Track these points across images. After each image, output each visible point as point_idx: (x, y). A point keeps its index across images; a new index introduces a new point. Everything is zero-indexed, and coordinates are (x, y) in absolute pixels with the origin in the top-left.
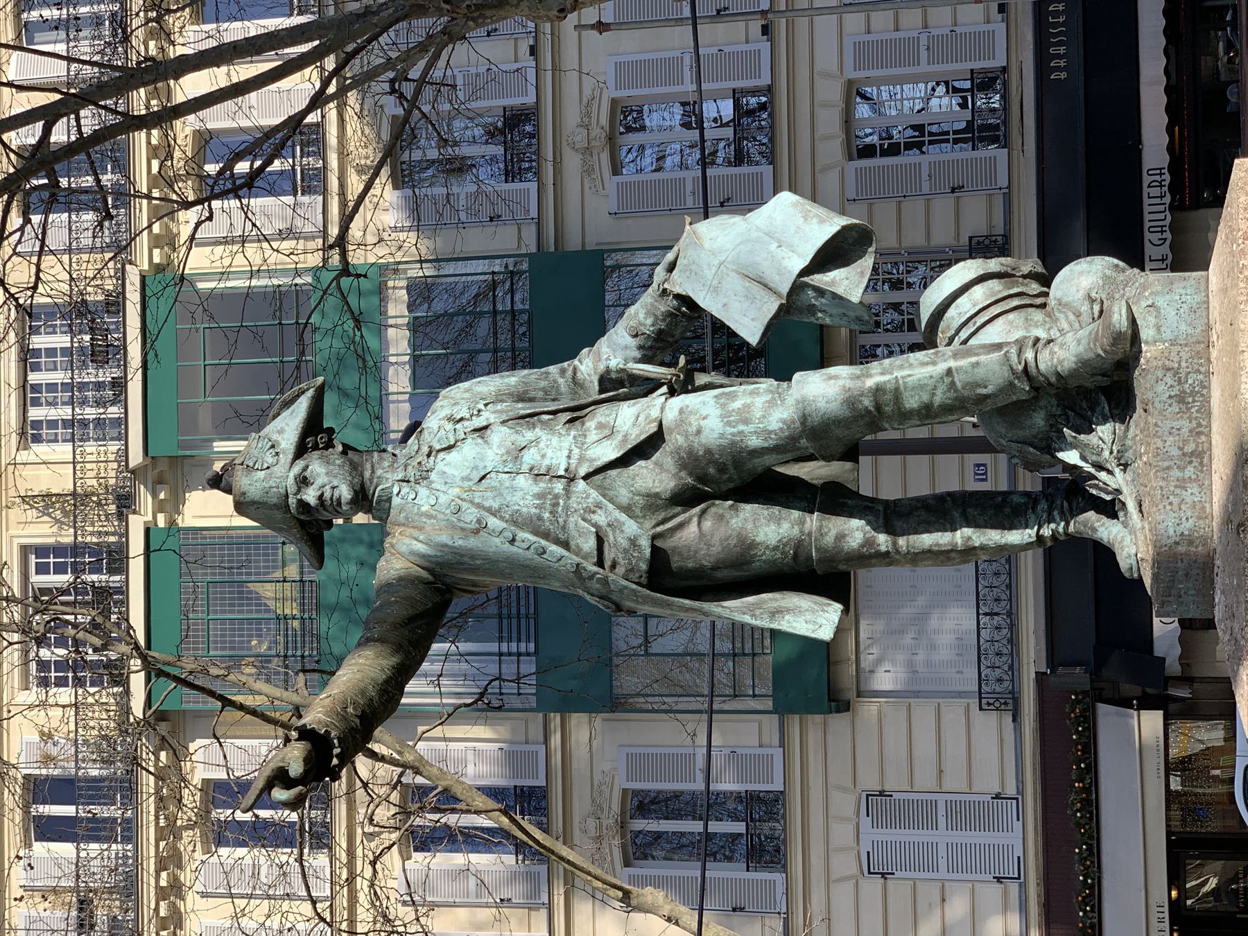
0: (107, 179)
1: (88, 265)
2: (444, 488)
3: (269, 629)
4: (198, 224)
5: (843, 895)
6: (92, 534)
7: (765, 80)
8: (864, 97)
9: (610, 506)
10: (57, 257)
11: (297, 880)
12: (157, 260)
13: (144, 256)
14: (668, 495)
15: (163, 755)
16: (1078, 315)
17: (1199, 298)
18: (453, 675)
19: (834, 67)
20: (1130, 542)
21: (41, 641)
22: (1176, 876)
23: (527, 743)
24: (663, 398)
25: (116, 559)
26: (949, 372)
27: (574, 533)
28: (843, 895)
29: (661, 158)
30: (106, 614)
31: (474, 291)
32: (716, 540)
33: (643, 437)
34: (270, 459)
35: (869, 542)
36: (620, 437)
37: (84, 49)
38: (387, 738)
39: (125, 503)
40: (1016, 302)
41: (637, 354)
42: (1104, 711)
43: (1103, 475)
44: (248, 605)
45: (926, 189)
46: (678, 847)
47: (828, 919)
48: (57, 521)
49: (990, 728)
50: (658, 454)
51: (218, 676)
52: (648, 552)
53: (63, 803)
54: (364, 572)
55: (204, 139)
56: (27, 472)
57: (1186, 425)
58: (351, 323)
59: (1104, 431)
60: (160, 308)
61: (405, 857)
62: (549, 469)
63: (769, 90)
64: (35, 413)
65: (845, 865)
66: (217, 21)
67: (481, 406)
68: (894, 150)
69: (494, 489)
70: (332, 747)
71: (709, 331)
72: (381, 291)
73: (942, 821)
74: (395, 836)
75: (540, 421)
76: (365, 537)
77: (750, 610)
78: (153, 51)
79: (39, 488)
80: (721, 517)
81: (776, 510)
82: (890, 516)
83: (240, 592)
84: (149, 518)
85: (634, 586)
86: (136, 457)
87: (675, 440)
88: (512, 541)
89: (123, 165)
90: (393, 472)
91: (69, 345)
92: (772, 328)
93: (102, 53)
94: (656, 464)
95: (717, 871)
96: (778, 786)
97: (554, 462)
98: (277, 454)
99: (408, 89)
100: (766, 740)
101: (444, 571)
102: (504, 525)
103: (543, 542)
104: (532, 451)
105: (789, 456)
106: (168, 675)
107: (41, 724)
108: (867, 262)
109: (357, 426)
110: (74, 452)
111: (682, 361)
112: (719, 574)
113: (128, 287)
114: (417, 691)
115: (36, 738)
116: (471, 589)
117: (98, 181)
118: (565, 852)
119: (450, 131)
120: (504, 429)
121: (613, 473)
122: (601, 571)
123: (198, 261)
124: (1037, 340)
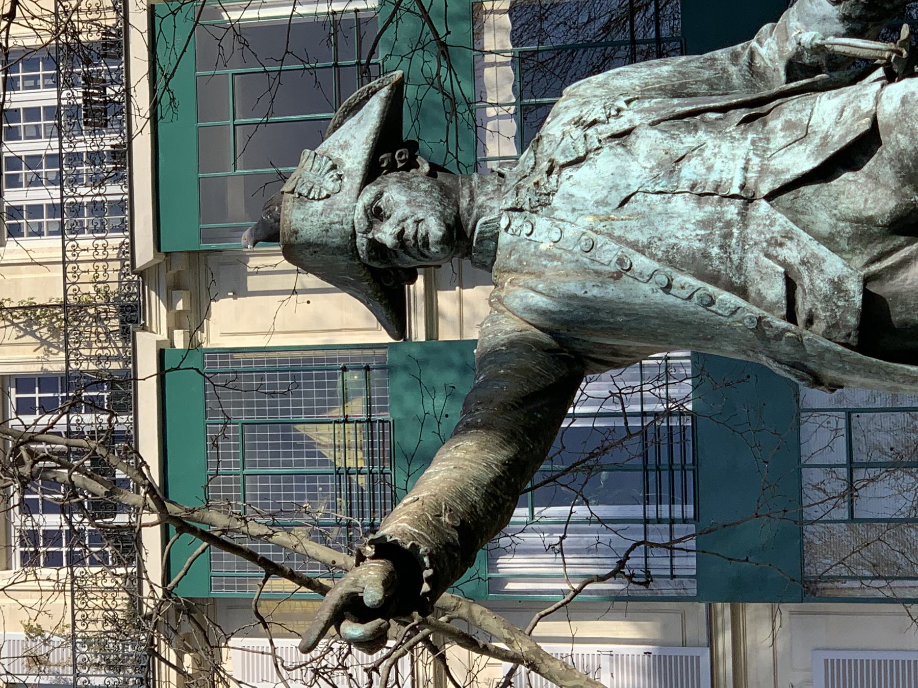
2: (571, 218)
3: (325, 488)
6: (89, 359)
9: (805, 236)
14: (886, 219)
23: (684, 644)
24: (878, 85)
27: (753, 275)
33: (849, 139)
34: (330, 185)
36: (817, 140)
39: (132, 316)
41: (840, 28)
44: (297, 455)
48: (43, 342)
50: (871, 162)
51: (259, 536)
52: (858, 299)
60: (176, 31)
62: (718, 186)
67: (621, 104)
69: (640, 215)
70: (421, 567)
75: (704, 121)
76: (456, 358)
83: (287, 437)
84: (163, 336)
85: (840, 348)
86: (145, 254)
87: (896, 141)
88: (667, 288)
90: (500, 199)
91: (55, 103)
94: (868, 176)
97: (725, 176)
98: (340, 177)
101: (573, 334)
102: (656, 265)
103: (711, 289)
104: (694, 161)
106: (193, 530)
110: (64, 247)
115: (22, 634)
120: (654, 133)
121: (808, 190)
122: (793, 327)
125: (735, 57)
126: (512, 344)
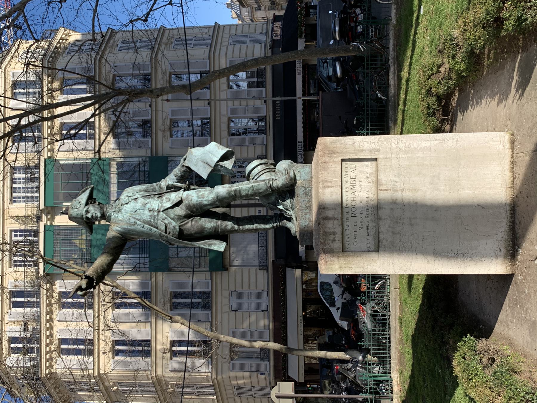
0: (36, 134)
1: (30, 156)
4: (60, 146)
5: (225, 316)
7: (209, 116)
8: (233, 121)
10: (22, 154)
11: (84, 316)
12: (49, 155)
13: (46, 154)
15: (48, 285)
16: (282, 173)
17: (310, 170)
18: (127, 263)
19: (225, 113)
20: (294, 227)
21: (15, 255)
22: (304, 310)
25: (36, 233)
26: (252, 186)
28: (225, 316)
29: (183, 134)
30: (33, 247)
31: (134, 165)
32: (195, 227)
34: (79, 206)
35: (233, 227)
37: (31, 100)
38: (109, 279)
39: (39, 219)
40: (268, 170)
41: (176, 181)
42: (287, 269)
43: (288, 211)
45: (247, 144)
46: (184, 306)
47: (221, 322)
49: (261, 274)
52: (178, 230)
53: (20, 298)
54: (104, 237)
55: (63, 125)
56: (12, 210)
57: (307, 200)
58: (101, 172)
59: (288, 201)
60: (50, 167)
61: (113, 310)
63: (210, 118)
64: (14, 195)
65: (226, 309)
66: (67, 94)
68: (240, 134)
69: (138, 214)
70: (94, 280)
71: (194, 177)
72: (109, 165)
73: (250, 297)
74: (110, 305)
77: (204, 244)
78: (49, 101)
79: (15, 214)
80: (197, 221)
81: (210, 219)
82: (238, 221)
86: (42, 207)
87: (185, 202)
88: (143, 227)
89: (40, 131)
92: (210, 175)
93: (35, 101)
95: (194, 312)
96: (210, 290)
99: (117, 113)
100: (207, 278)
105: (213, 206)
106: (50, 263)
107: (15, 277)
108: (233, 160)
109: (102, 199)
111: (187, 183)
112: (196, 235)
113: (41, 162)
114: (116, 267)
116: (132, 239)
117: (34, 134)
118: (155, 307)
119: (129, 124)
120: (142, 199)
121: (170, 210)
123: (60, 156)
124: (273, 179)
125: (157, 185)
126: (113, 237)
